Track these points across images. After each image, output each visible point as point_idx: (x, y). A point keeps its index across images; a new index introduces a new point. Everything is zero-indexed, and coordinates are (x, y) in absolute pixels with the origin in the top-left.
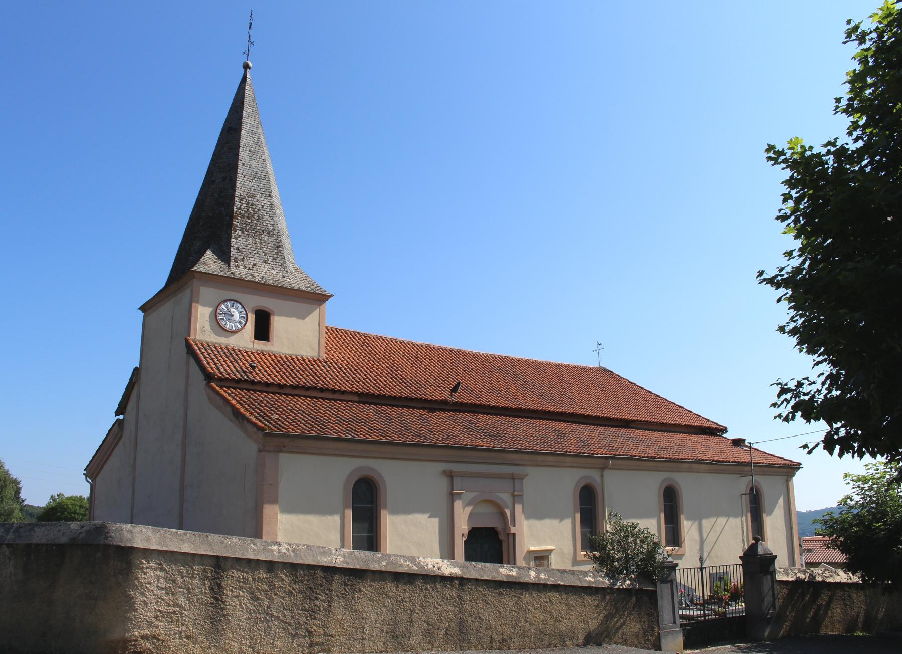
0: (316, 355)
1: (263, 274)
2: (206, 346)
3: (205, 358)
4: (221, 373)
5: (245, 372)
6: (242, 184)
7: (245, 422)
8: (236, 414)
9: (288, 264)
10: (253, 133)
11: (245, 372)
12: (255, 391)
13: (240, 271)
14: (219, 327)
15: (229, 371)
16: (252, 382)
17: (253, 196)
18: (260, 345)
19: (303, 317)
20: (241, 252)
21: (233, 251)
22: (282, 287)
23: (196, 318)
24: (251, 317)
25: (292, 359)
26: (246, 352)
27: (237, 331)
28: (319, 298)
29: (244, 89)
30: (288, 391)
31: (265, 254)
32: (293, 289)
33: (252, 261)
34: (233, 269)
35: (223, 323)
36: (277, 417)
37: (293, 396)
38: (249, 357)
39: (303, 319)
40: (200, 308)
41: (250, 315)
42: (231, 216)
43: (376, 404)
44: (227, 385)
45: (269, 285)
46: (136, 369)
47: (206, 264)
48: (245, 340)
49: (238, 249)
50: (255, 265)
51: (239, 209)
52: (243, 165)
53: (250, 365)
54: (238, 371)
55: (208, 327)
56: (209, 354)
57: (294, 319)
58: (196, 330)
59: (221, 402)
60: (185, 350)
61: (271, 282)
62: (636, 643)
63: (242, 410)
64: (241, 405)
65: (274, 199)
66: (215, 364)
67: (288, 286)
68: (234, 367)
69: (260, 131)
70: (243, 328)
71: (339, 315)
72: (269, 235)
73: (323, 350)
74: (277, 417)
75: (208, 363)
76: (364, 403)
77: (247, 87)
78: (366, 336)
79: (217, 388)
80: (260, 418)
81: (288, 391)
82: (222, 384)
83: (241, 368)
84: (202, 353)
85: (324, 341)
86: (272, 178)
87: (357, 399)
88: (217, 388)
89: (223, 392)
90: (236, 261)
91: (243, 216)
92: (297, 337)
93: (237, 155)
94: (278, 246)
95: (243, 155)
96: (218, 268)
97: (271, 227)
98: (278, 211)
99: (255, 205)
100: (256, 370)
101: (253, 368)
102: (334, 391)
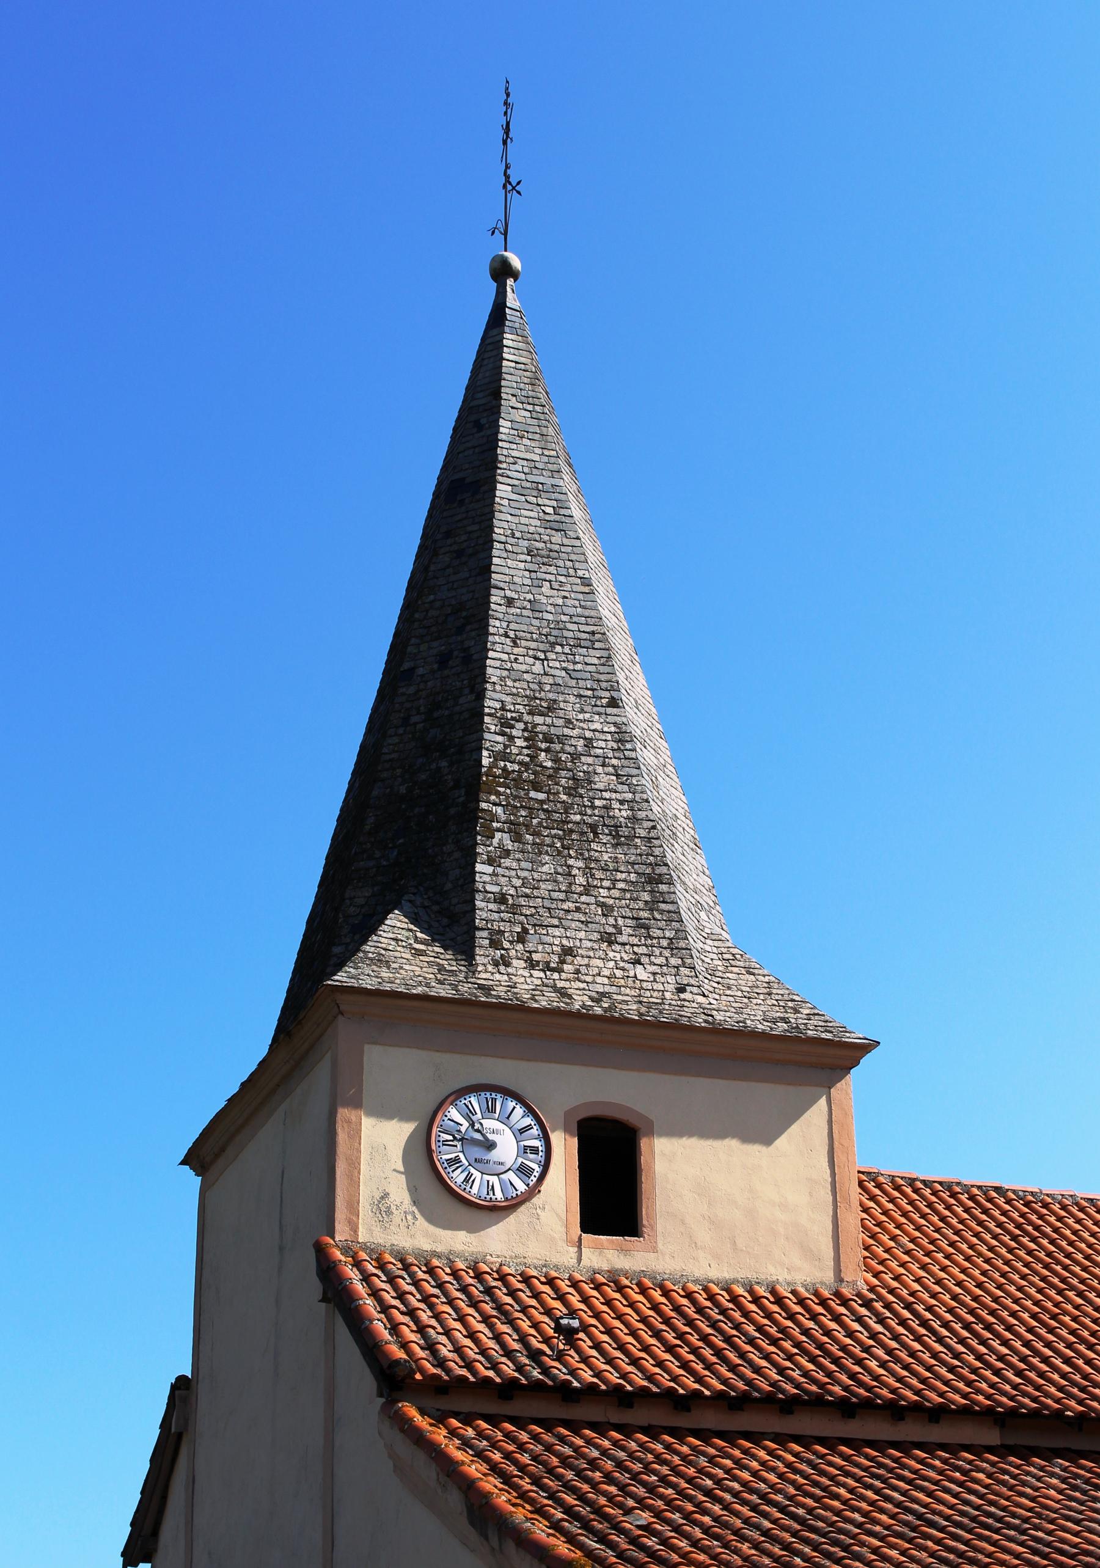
0: (829, 1276)
1: (601, 985)
2: (396, 1268)
3: (385, 1309)
4: (441, 1363)
5: (535, 1355)
6: (509, 669)
7: (510, 1546)
8: (481, 1514)
9: (695, 942)
10: (539, 489)
11: (535, 1355)
12: (575, 1427)
13: (521, 982)
14: (450, 1201)
15: (472, 1353)
16: (564, 1392)
17: (552, 708)
18: (605, 1254)
19: (764, 1133)
20: (515, 909)
21: (484, 910)
22: (675, 1026)
23: (354, 1164)
24: (565, 1148)
25: (734, 1299)
26: (551, 1282)
27: (513, 1205)
28: (819, 1059)
29: (499, 346)
30: (709, 1420)
31: (607, 910)
32: (716, 1031)
33: (556, 937)
34: (486, 973)
35: (457, 1177)
36: (645, 1517)
37: (730, 1437)
38: (561, 1297)
39: (768, 1141)
40: (368, 1123)
41: (558, 1139)
42: (473, 784)
43: (1073, 1455)
44: (466, 1405)
45: (624, 1021)
46: (181, 1385)
47: (381, 961)
48: (545, 1233)
49: (501, 899)
50: (568, 952)
51: (504, 756)
52: (510, 602)
53: (559, 1328)
54: (509, 1353)
55: (399, 1193)
56: (401, 1296)
57: (733, 1143)
58: (353, 1207)
59: (429, 1472)
60: (315, 1287)
61: (632, 1010)
62: (488, 341)
63: (502, 1500)
64: (506, 1479)
65: (630, 712)
66: (421, 1329)
67: (700, 1021)
68: (498, 1337)
69: (566, 481)
70: (533, 1191)
71: (914, 1117)
72: (619, 837)
73: (854, 1256)
74: (645, 1517)
75: (394, 1328)
76: (1026, 1453)
77: (509, 340)
78: (1030, 1201)
79: (418, 1419)
80: (574, 1528)
81: (709, 1420)
82: (445, 1403)
83: (523, 1339)
84: (375, 1293)
85: (852, 1219)
86: (622, 643)
87: (993, 1437)
88: (418, 1419)
89: (440, 1435)
90: (495, 944)
91: (518, 782)
92: (745, 1212)
93: (486, 570)
94: (656, 879)
95: (508, 568)
96: (430, 973)
97: (622, 813)
98: (646, 756)
99: (562, 739)
100: (585, 1344)
101: (570, 1334)
102: (895, 1410)
